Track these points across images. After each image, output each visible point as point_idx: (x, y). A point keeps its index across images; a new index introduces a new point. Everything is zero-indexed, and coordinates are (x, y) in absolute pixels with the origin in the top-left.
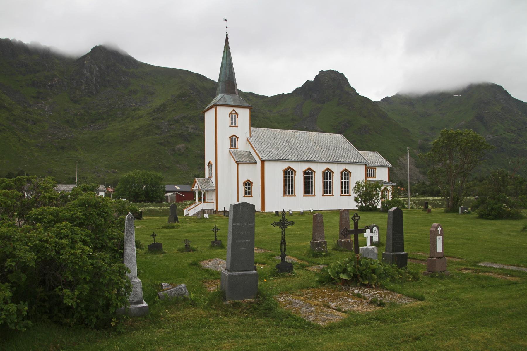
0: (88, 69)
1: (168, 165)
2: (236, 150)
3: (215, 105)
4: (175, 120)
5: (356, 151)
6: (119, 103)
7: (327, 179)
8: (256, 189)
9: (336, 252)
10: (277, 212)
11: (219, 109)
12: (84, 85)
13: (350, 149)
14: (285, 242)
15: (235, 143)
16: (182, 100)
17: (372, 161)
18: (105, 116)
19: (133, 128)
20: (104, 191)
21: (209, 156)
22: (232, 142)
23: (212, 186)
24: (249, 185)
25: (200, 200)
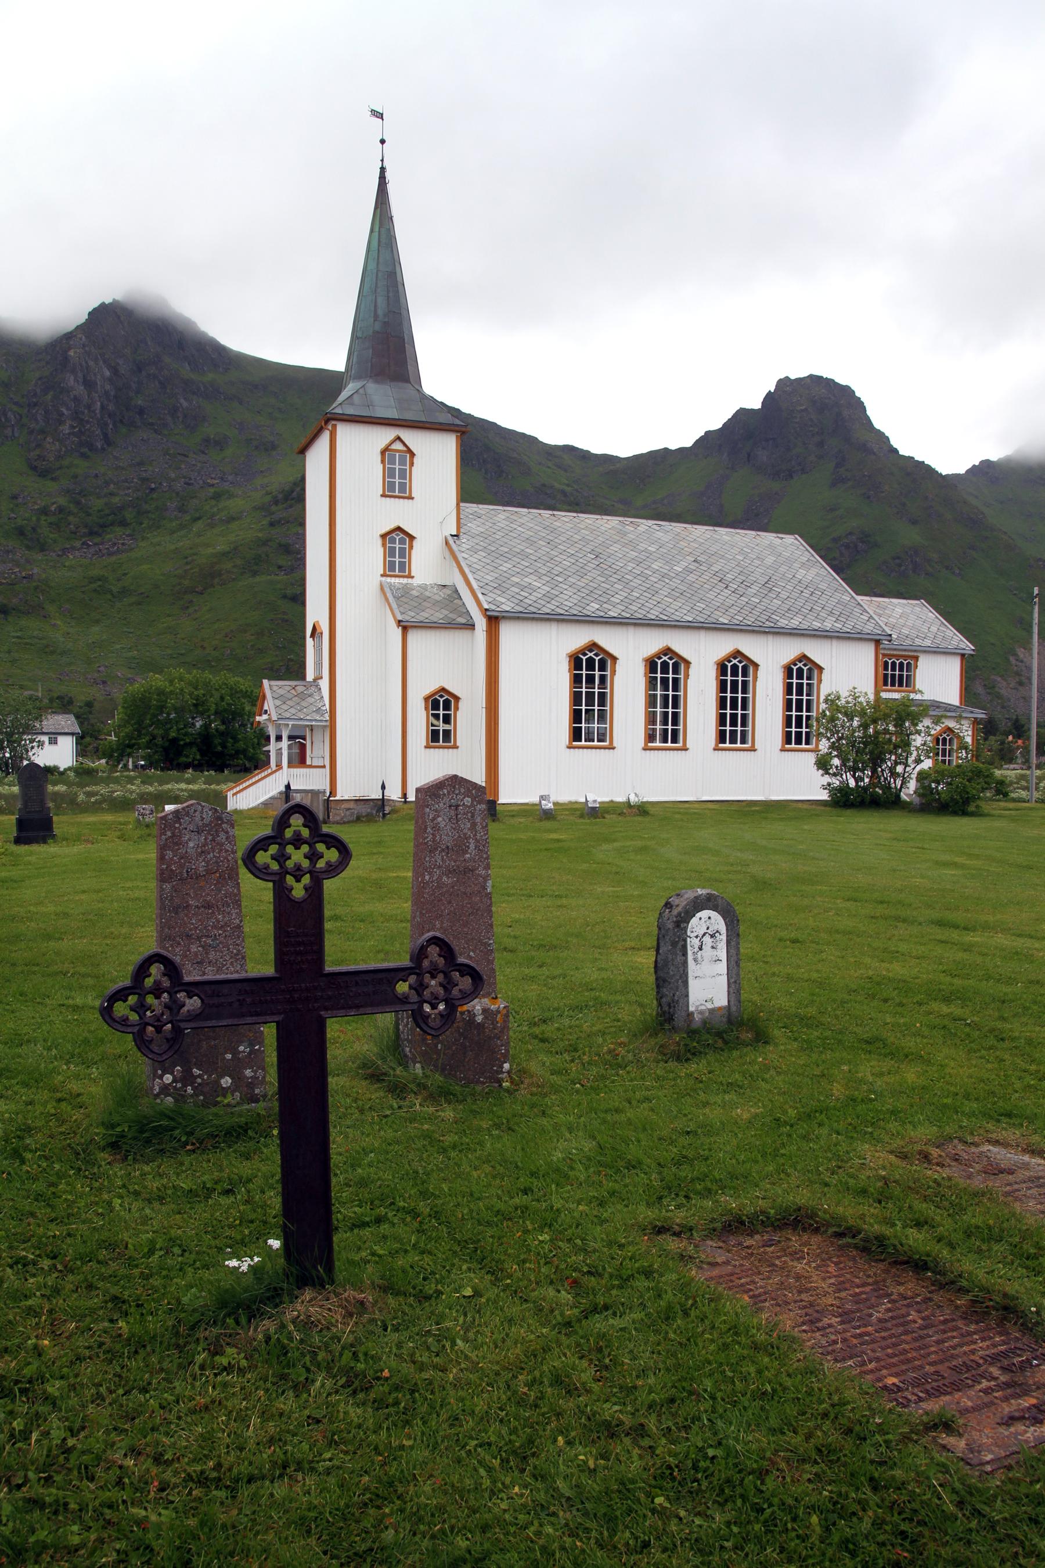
0: (80, 375)
2: (404, 581)
5: (845, 593)
6: (173, 475)
7: (734, 690)
8: (469, 721)
11: (345, 433)
12: (68, 422)
13: (823, 586)
17: (905, 631)
18: (129, 515)
19: (210, 550)
20: (72, 734)
22: (392, 552)
24: (447, 705)
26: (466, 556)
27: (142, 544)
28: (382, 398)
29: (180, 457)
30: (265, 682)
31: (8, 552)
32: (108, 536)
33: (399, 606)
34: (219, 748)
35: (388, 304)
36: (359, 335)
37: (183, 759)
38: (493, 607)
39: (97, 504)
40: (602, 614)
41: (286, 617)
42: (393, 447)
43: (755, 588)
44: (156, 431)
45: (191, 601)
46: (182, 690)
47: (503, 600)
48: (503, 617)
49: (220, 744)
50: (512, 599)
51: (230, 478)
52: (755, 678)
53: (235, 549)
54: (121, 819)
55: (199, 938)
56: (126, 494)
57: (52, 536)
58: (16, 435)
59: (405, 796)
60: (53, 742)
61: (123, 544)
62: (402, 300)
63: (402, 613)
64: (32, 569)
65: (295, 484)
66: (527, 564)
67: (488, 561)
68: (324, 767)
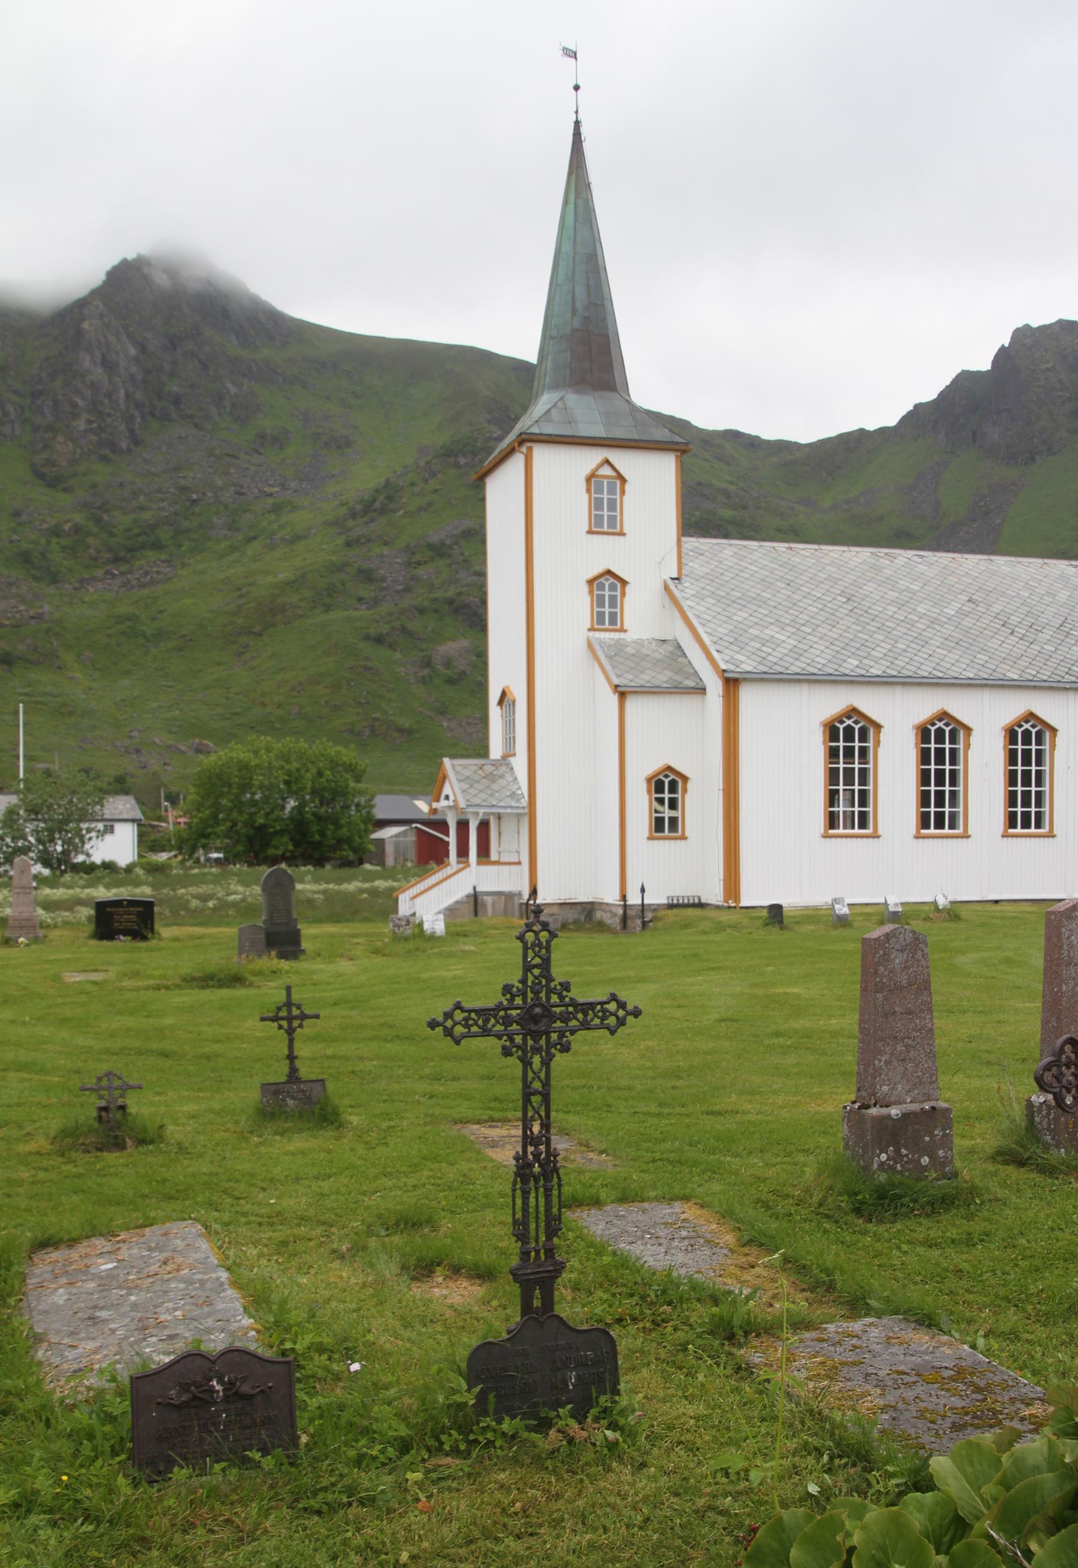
0: (98, 354)
1: (405, 722)
2: (616, 636)
3: (527, 439)
4: (431, 547)
6: (219, 482)
8: (702, 806)
9: (1012, 1172)
10: (776, 911)
11: (542, 455)
12: (84, 416)
14: (550, 1167)
15: (613, 604)
16: (457, 465)
18: (164, 534)
19: (270, 579)
20: (133, 821)
21: (504, 670)
22: (600, 601)
23: (513, 795)
25: (463, 852)
26: (692, 604)
27: (183, 572)
28: (586, 412)
29: (228, 459)
30: (447, 762)
31: (10, 584)
32: (138, 563)
33: (614, 667)
34: (317, 837)
35: (589, 294)
36: (554, 333)
37: (271, 852)
38: (732, 667)
39: (123, 520)
40: (863, 672)
41: (370, 664)
42: (601, 472)
43: (1044, 636)
44: (196, 425)
45: (247, 646)
46: (270, 763)
47: (743, 658)
48: (745, 679)
49: (318, 831)
50: (753, 657)
51: (293, 485)
52: (1053, 746)
53: (303, 576)
54: (346, 931)
55: (902, 1039)
56: (160, 508)
57: (65, 563)
58: (17, 432)
59: (624, 898)
60: (110, 830)
61: (158, 573)
62: (605, 288)
63: (618, 676)
64: (42, 607)
65: (377, 491)
66: (766, 612)
67: (719, 610)
68: (519, 863)
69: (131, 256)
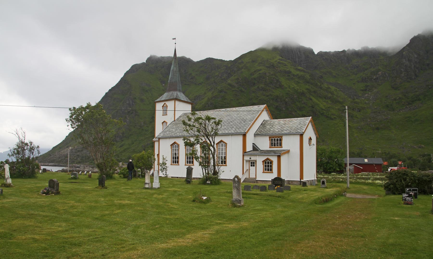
69: (416, 35)
